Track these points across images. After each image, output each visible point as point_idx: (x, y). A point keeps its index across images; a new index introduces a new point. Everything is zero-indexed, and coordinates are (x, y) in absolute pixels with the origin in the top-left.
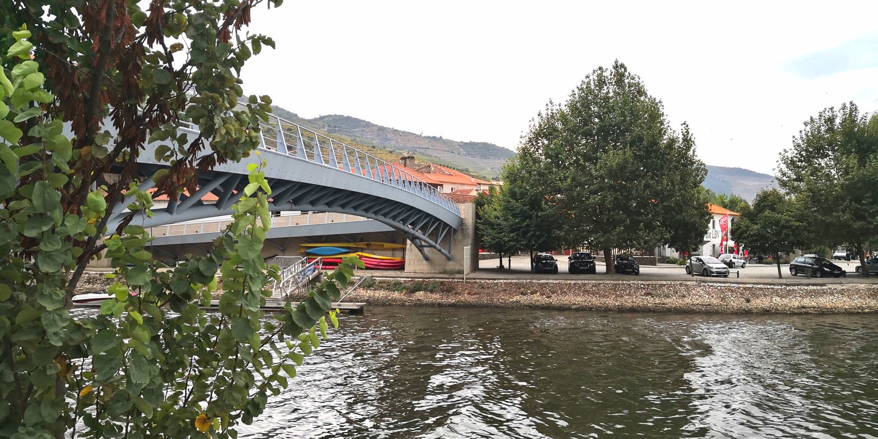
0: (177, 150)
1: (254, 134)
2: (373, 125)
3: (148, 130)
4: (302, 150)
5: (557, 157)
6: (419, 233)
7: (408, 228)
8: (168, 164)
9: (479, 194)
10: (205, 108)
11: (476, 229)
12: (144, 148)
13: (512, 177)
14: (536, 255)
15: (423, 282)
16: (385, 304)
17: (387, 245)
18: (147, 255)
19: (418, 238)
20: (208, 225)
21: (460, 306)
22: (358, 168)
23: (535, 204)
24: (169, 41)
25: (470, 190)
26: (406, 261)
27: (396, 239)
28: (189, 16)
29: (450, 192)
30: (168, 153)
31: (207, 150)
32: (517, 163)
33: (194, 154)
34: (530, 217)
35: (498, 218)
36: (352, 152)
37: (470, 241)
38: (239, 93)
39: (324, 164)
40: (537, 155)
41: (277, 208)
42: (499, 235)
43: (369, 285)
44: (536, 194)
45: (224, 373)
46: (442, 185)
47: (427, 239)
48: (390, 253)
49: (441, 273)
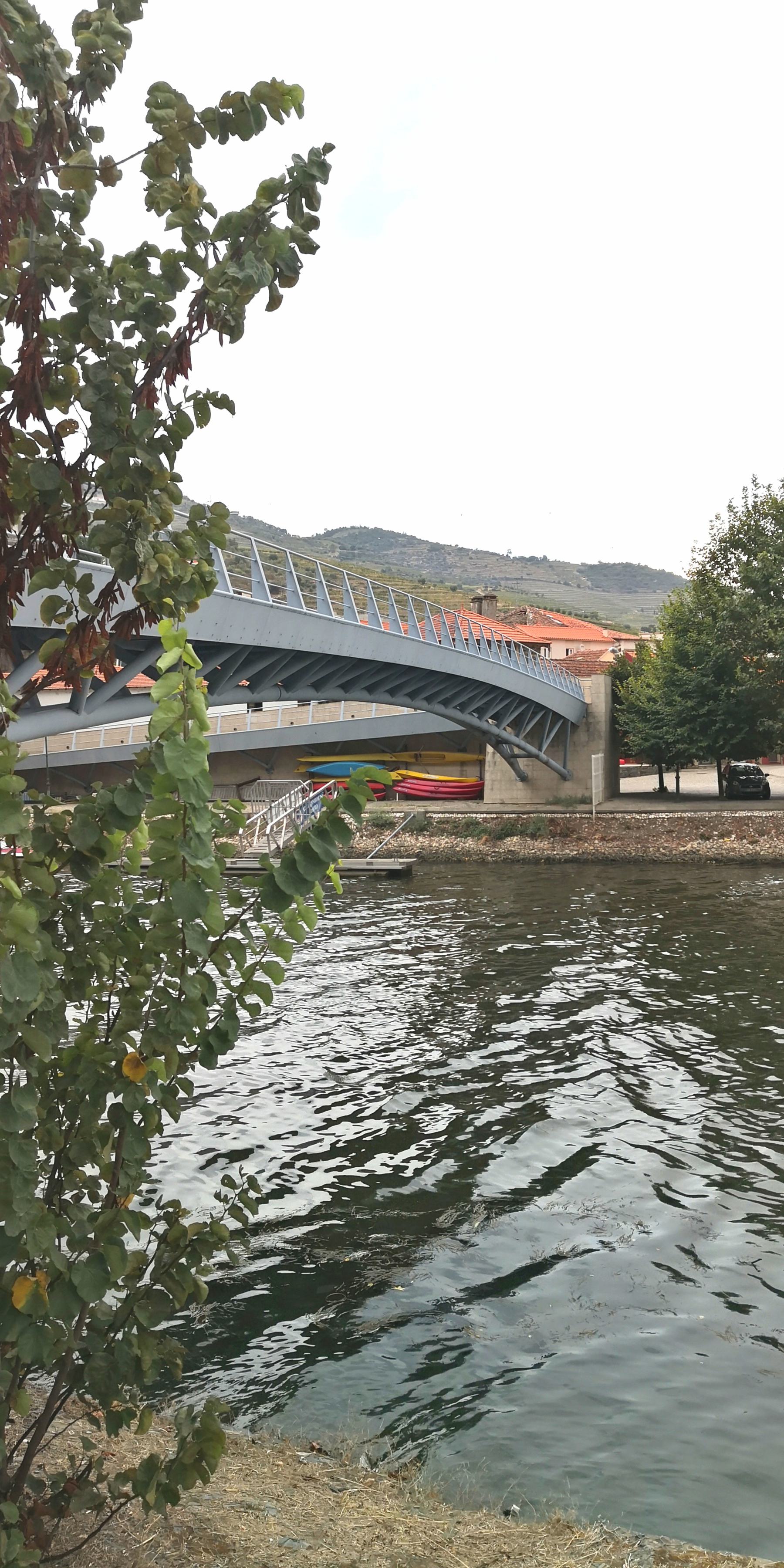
0: (77, 603)
1: (206, 568)
2: (421, 542)
3: (27, 572)
4: (295, 592)
5: (766, 583)
6: (508, 734)
7: (488, 724)
8: (63, 627)
9: (617, 658)
10: (122, 527)
11: (613, 721)
12: (21, 604)
13: (679, 624)
14: (728, 766)
15: (517, 820)
16: (452, 859)
17: (450, 756)
18: (19, 783)
19: (507, 742)
20: (120, 732)
21: (586, 862)
22: (395, 620)
23: (723, 672)
24: (55, 416)
25: (602, 652)
26: (486, 783)
27: (467, 744)
28: (84, 367)
29: (563, 656)
30: (63, 610)
31: (127, 602)
32: (688, 598)
33: (107, 609)
34: (715, 697)
35: (655, 701)
36: (384, 593)
37: (602, 744)
38: (177, 497)
39: (335, 616)
40: (725, 582)
41: (256, 697)
42: (657, 732)
43: (420, 826)
44: (727, 654)
45: (165, 982)
46: (548, 645)
47: (523, 743)
48: (458, 768)
49: (548, 803)
